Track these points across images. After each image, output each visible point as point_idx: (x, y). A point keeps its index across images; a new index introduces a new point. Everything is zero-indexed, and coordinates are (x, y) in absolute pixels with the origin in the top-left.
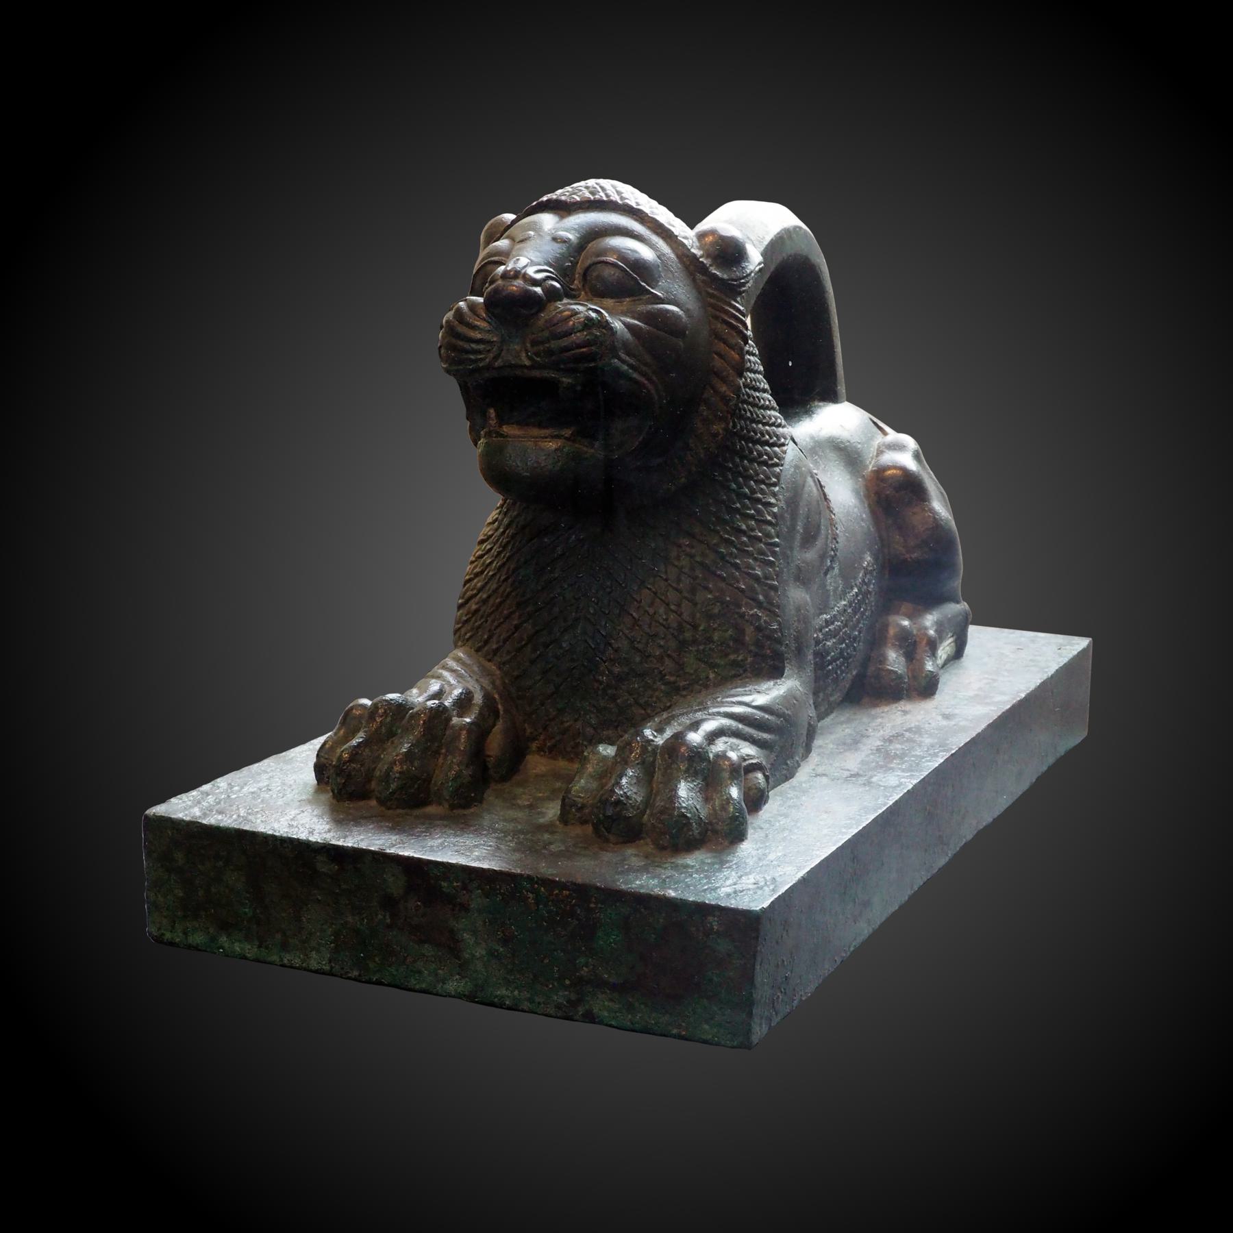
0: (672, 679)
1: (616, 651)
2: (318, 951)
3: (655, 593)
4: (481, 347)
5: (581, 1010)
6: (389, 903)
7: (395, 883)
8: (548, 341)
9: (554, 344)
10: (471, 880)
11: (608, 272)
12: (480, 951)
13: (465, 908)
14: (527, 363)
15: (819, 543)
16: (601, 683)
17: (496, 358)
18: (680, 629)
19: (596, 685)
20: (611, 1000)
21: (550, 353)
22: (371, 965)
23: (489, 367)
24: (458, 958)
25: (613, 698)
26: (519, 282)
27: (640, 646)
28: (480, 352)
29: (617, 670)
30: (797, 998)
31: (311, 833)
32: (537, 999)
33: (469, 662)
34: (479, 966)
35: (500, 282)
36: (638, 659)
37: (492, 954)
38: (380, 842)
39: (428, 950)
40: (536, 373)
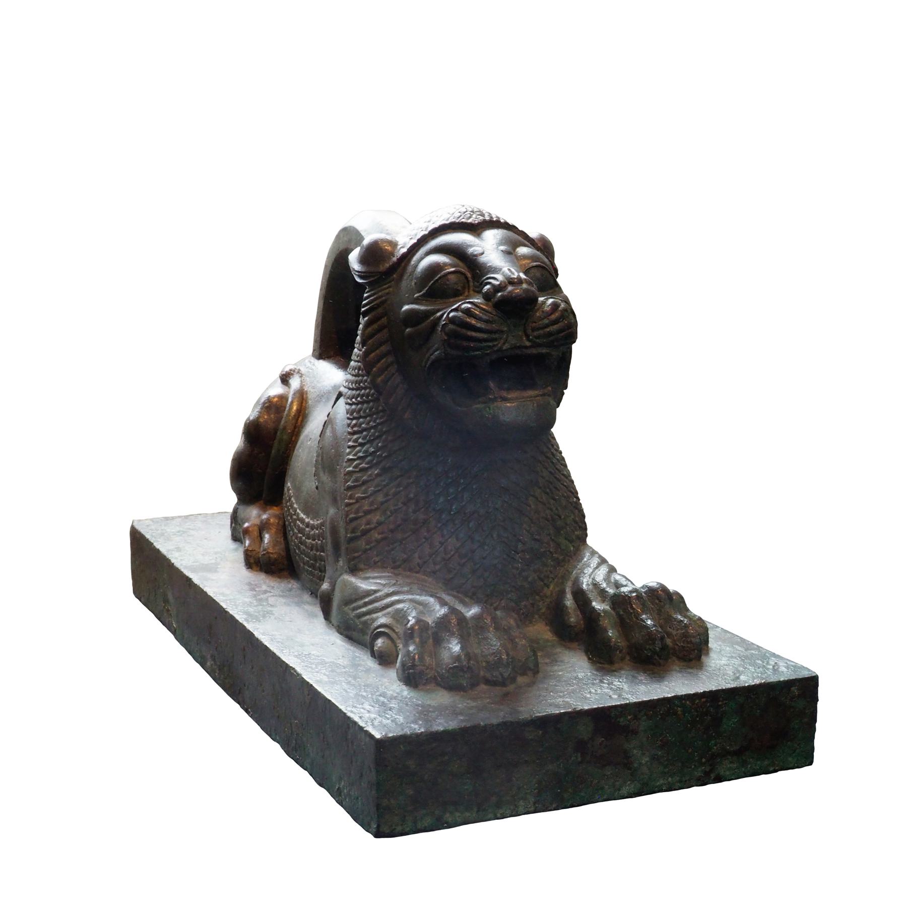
2: (525, 799)
4: (497, 336)
5: (713, 776)
6: (581, 746)
7: (584, 730)
10: (640, 711)
12: (645, 760)
13: (635, 732)
14: (528, 344)
16: (517, 569)
17: (504, 344)
19: (514, 571)
20: (731, 762)
22: (566, 796)
24: (629, 769)
25: (526, 578)
27: (537, 537)
28: (496, 340)
31: (754, 678)
32: (684, 779)
34: (645, 769)
35: (510, 288)
37: (654, 758)
39: (608, 771)
40: (534, 351)
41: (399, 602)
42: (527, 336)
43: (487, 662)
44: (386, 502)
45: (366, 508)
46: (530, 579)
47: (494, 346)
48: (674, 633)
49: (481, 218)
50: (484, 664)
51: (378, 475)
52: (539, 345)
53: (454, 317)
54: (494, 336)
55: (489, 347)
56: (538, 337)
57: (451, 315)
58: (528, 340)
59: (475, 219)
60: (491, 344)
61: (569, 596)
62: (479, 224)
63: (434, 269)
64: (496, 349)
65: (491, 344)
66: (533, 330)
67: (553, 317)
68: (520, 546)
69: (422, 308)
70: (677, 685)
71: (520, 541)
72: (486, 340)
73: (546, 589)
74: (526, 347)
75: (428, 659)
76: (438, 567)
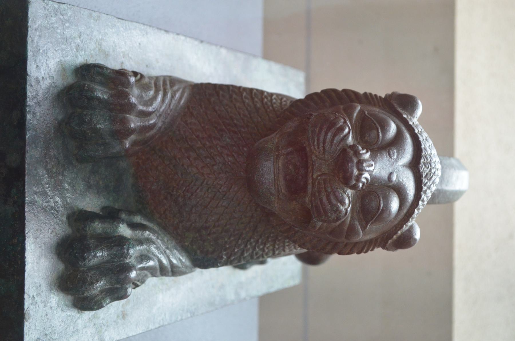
0: (180, 227)
1: (189, 198)
3: (222, 215)
4: (321, 149)
8: (326, 191)
9: (323, 195)
11: (374, 204)
14: (315, 176)
15: (342, 112)
16: (173, 191)
17: (316, 156)
18: (206, 228)
21: (320, 192)
23: (312, 153)
25: (166, 198)
26: (356, 172)
27: (194, 211)
28: (318, 148)
29: (180, 199)
30: (64, 314)
33: (171, 107)
35: (355, 160)
36: (187, 209)
38: (95, 261)
40: (310, 181)
41: (163, 100)
42: (320, 176)
43: (85, 115)
44: (235, 107)
45: (234, 96)
46: (165, 201)
47: (314, 146)
48: (90, 274)
49: (424, 175)
50: (85, 113)
51: (255, 105)
52: (313, 184)
53: (340, 120)
54: (321, 145)
55: (314, 143)
56: (319, 183)
57: (347, 130)
58: (317, 177)
59: (424, 170)
60: (316, 143)
61: (145, 222)
62: (419, 170)
63: (384, 127)
64: (312, 148)
65: (316, 143)
66: (324, 180)
67: (332, 197)
68: (189, 195)
69: (355, 115)
70: (38, 264)
71: (192, 195)
72: (318, 140)
73: (158, 216)
74: (312, 175)
75: (99, 78)
76: (182, 132)
